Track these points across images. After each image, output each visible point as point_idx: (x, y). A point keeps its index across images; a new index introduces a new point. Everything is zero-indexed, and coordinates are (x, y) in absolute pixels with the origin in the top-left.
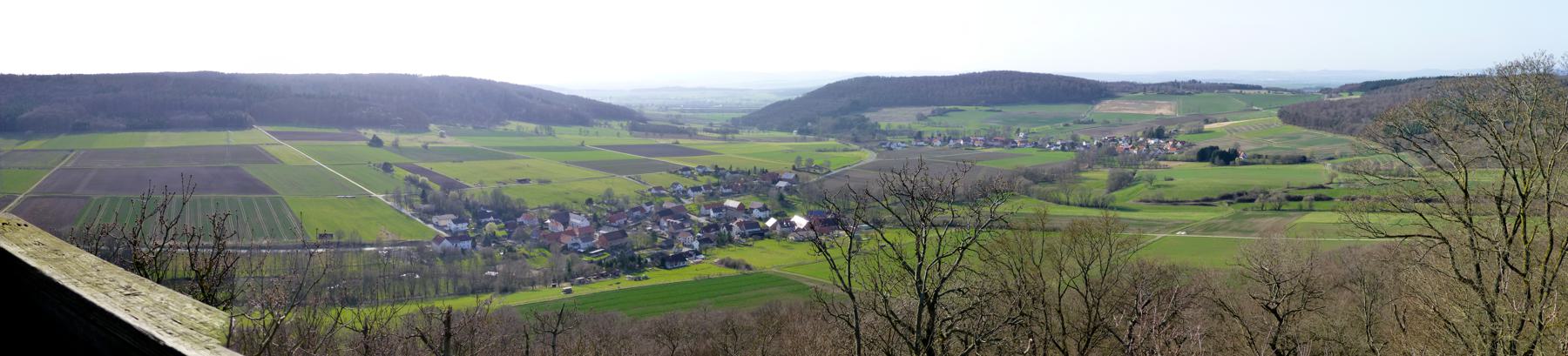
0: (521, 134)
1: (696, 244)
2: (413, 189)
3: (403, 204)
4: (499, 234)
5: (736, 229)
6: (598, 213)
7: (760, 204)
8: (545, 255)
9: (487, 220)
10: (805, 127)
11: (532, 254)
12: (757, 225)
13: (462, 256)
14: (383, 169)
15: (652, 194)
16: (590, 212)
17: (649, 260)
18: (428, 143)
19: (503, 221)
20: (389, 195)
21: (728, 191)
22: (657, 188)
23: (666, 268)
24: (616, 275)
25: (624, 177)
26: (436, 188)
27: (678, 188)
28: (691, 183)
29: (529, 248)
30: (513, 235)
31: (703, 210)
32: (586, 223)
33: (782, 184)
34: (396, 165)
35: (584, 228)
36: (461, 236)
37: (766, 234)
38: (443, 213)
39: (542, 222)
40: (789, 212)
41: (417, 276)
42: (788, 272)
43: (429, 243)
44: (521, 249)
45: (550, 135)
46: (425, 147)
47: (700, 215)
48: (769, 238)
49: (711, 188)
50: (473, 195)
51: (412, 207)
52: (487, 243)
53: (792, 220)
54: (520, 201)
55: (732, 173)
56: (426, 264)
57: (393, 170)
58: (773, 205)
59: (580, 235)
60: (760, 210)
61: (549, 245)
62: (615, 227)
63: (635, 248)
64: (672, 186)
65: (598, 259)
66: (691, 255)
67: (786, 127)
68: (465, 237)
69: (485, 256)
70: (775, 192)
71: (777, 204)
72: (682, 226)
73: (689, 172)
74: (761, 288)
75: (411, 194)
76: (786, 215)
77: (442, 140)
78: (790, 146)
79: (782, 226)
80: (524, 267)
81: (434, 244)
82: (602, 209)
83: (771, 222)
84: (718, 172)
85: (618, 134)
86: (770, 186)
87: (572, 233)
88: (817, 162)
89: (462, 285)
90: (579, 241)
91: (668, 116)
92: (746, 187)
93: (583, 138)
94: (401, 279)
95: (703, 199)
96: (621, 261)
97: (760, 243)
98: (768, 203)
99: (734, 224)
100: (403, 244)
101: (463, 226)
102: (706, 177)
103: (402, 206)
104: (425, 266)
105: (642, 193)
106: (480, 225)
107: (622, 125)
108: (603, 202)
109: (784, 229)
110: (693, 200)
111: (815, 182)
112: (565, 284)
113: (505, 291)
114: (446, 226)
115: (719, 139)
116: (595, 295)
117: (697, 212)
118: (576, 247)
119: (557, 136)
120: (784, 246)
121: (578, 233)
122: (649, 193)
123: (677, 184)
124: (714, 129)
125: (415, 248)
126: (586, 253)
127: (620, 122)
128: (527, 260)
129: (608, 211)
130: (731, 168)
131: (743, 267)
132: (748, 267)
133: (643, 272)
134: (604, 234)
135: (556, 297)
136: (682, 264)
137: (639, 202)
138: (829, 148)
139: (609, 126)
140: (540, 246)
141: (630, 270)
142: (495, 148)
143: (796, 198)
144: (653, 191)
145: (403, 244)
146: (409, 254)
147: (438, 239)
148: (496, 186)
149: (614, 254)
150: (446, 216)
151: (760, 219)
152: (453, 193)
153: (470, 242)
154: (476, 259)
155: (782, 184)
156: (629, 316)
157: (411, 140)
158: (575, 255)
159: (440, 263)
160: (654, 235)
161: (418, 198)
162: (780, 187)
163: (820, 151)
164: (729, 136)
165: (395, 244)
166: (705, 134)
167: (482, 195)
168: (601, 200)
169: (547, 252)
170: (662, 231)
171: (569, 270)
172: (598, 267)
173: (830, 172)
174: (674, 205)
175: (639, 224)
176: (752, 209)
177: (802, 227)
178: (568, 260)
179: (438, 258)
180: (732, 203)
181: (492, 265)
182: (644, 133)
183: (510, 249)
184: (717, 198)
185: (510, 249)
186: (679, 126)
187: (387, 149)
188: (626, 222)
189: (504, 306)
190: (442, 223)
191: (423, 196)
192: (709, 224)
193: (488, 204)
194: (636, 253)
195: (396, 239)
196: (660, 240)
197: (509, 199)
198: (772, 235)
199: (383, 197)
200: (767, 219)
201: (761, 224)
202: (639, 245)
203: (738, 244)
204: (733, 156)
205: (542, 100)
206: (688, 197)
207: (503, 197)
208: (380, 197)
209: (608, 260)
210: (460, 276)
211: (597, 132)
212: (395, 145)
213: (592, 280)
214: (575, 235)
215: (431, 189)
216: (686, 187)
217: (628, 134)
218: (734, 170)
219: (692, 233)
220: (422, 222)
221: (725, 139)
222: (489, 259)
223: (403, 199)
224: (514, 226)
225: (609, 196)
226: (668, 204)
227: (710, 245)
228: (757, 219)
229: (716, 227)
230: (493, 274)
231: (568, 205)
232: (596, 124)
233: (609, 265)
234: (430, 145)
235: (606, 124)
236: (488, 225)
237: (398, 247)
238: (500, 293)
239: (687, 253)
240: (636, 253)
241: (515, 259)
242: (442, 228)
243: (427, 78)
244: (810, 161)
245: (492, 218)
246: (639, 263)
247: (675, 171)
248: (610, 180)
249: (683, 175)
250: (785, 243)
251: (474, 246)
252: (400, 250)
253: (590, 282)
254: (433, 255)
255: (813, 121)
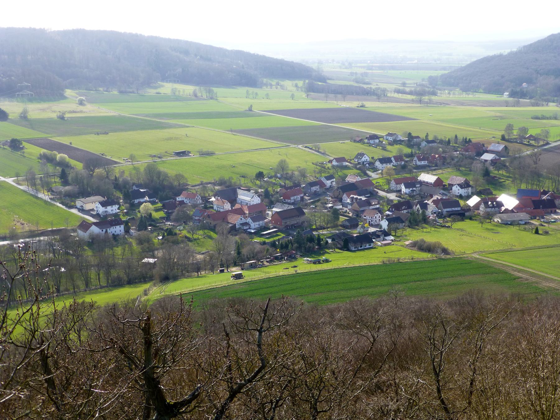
0: (176, 98)
1: (385, 224)
2: (50, 168)
3: (39, 187)
4: (157, 215)
5: (431, 207)
6: (270, 189)
7: (461, 179)
8: (210, 237)
9: (142, 200)
10: (518, 89)
11: (195, 236)
12: (457, 204)
13: (115, 243)
14: (10, 146)
15: (333, 166)
16: (260, 187)
17: (330, 241)
18: (64, 113)
19: (161, 201)
20: (20, 178)
21: (423, 163)
22: (338, 160)
23: (349, 250)
24: (292, 258)
25: (300, 146)
26: (79, 166)
27: (363, 159)
28: (378, 153)
29: (192, 231)
30: (172, 217)
31: (393, 185)
32: (257, 200)
33: (488, 157)
34: (25, 141)
35: (254, 205)
36: (112, 221)
37: (467, 214)
38: (88, 195)
39: (206, 200)
40: (495, 189)
41: (63, 270)
42: (492, 258)
43: (74, 231)
44: (183, 231)
45: (212, 98)
46: (62, 118)
47: (389, 191)
48: (471, 219)
49: (403, 160)
50: (123, 172)
51: (50, 190)
52: (142, 226)
53: (498, 200)
54: (179, 177)
55: (429, 142)
56: (72, 255)
57: (23, 148)
58: (476, 181)
59: (249, 214)
60: (461, 186)
61: (215, 226)
62: (289, 204)
63: (314, 227)
64: (356, 157)
65: (272, 240)
66: (378, 236)
67: (496, 89)
68: (115, 221)
69: (140, 242)
70: (479, 166)
71: (481, 180)
72: (368, 203)
73: (377, 141)
74: (460, 275)
75: (48, 175)
76: (491, 193)
77: (81, 108)
78: (500, 111)
79: (487, 206)
80: (187, 251)
81: (80, 232)
82: (275, 184)
83: (474, 201)
84: (411, 141)
85: (293, 97)
86: (473, 159)
87: (240, 212)
88: (532, 132)
89: (116, 275)
90: (249, 220)
91: (352, 74)
92: (444, 158)
93: (250, 101)
94: (43, 274)
95: (393, 172)
96: (297, 242)
97: (460, 225)
98: (470, 178)
99: (430, 202)
100: (43, 233)
101: (113, 209)
102: (397, 147)
103: (37, 190)
104: (71, 258)
105: (322, 165)
106: (134, 207)
107: (296, 86)
108: (276, 176)
109: (489, 210)
110: (382, 174)
111: (528, 155)
112: (234, 269)
113: (166, 279)
114: (93, 210)
115: (413, 101)
116: (269, 279)
117: (386, 187)
118: (245, 228)
119: (220, 99)
120: (487, 229)
121: (247, 212)
122: (329, 165)
123: (362, 155)
124: (408, 90)
125: (57, 237)
126: (258, 233)
127: (295, 82)
128: (190, 244)
129: (281, 186)
130: (427, 136)
131: (439, 251)
132: (445, 251)
133: (323, 254)
134: (277, 212)
135: (225, 283)
136: (368, 246)
137: (318, 176)
138: (548, 115)
139: (282, 87)
140: (204, 228)
141: (308, 252)
142: (147, 116)
143: (504, 173)
144: (335, 163)
145: (43, 233)
146: (51, 245)
147: (85, 226)
148: (150, 160)
149: (289, 235)
150: (92, 198)
151: (461, 197)
152: (98, 171)
153: (122, 226)
154: (130, 244)
155: (488, 157)
156: (309, 302)
157: (43, 110)
158: (245, 236)
159: (88, 253)
160: (336, 213)
161: (57, 180)
162: (486, 161)
163: (537, 118)
164: (426, 98)
165: (32, 234)
166: (396, 95)
167: (134, 172)
168: (273, 174)
169: (212, 234)
170: (345, 209)
171: (239, 253)
172: (271, 250)
173: (548, 144)
174: (359, 179)
175: (318, 201)
176: (451, 185)
177: (510, 209)
178: (236, 242)
179: (86, 248)
180: (428, 178)
181: (150, 251)
182: (323, 95)
183: (170, 232)
184: (410, 172)
185: (170, 232)
186: (365, 86)
187: (14, 122)
188: (302, 198)
189: (166, 295)
190: (88, 207)
191: (63, 176)
192: (399, 201)
193: (141, 181)
194: (314, 233)
195: (34, 228)
196: (342, 218)
197: (166, 175)
198: (475, 216)
199: (14, 181)
200: (468, 197)
201: (462, 203)
202: (318, 224)
203: (433, 224)
204: (429, 122)
205: (201, 57)
206: (375, 170)
207: (159, 173)
208: (10, 181)
209: (283, 241)
210: (113, 266)
211: (267, 95)
212: (24, 117)
213: (265, 263)
214: (245, 214)
215: (72, 168)
216: (373, 158)
217: (304, 95)
218: (430, 138)
219: (380, 211)
220: (64, 207)
221: (420, 101)
222: (146, 245)
223: (38, 182)
224: (174, 206)
225: (283, 169)
226: (352, 178)
227: (401, 225)
228: (457, 196)
229: (409, 205)
230: (151, 260)
231: (235, 179)
232: (266, 85)
233: (284, 247)
234: (67, 116)
235: (278, 84)
236: (142, 206)
237: (38, 238)
238: (161, 282)
239: (374, 234)
240: (314, 233)
241: (176, 243)
242: (88, 212)
243: (59, 33)
244: (524, 130)
245: (147, 198)
246: (319, 244)
247: (359, 139)
248: (283, 150)
249: (370, 145)
250: (489, 226)
251: (127, 231)
252: (40, 241)
253: (263, 266)
254: (80, 243)
255: (530, 81)
